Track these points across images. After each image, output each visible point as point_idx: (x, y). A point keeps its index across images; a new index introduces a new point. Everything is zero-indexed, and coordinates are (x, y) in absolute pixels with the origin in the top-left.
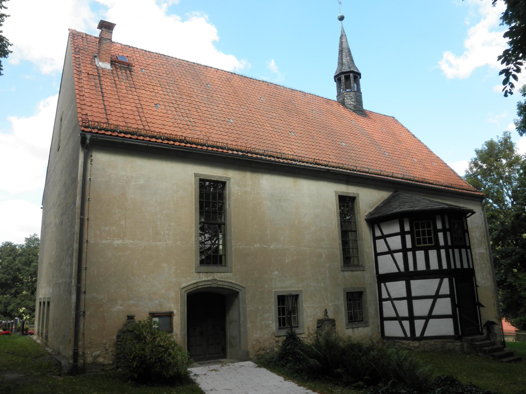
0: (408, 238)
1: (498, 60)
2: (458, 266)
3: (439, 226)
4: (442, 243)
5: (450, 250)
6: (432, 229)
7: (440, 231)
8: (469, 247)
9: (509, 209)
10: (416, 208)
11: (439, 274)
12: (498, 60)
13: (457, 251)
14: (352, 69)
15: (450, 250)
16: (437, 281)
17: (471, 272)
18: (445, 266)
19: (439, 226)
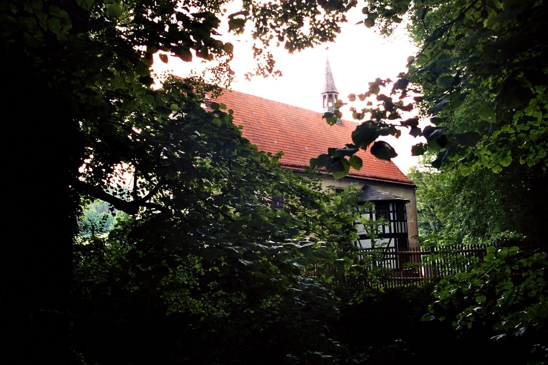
0: (374, 215)
1: (398, 77)
2: (400, 232)
3: (391, 209)
4: (392, 219)
5: (396, 223)
6: (387, 210)
7: (391, 212)
8: (406, 221)
9: (494, 218)
10: (380, 199)
11: (390, 236)
12: (398, 77)
13: (399, 223)
14: (334, 91)
15: (396, 223)
16: (389, 239)
17: (406, 235)
18: (393, 232)
19: (391, 209)
